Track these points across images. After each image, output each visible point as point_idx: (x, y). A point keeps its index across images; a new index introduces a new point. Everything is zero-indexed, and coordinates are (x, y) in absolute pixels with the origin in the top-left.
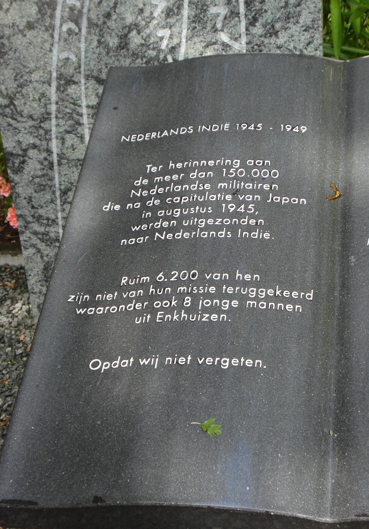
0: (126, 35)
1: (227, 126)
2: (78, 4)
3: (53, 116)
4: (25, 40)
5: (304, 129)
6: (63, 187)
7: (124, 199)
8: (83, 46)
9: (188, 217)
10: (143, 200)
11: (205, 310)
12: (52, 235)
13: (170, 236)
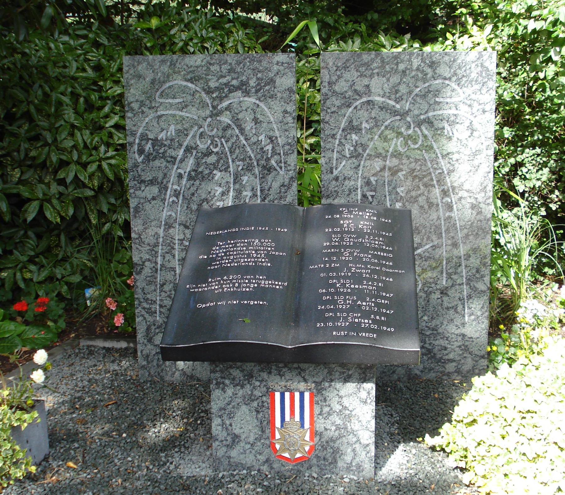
0: (201, 204)
1: (253, 228)
2: (179, 188)
3: (160, 244)
4: (151, 205)
5: (286, 230)
6: (161, 283)
7: (208, 255)
8: (179, 209)
9: (237, 258)
10: (217, 254)
11: (243, 287)
12: (153, 309)
13: (229, 265)
